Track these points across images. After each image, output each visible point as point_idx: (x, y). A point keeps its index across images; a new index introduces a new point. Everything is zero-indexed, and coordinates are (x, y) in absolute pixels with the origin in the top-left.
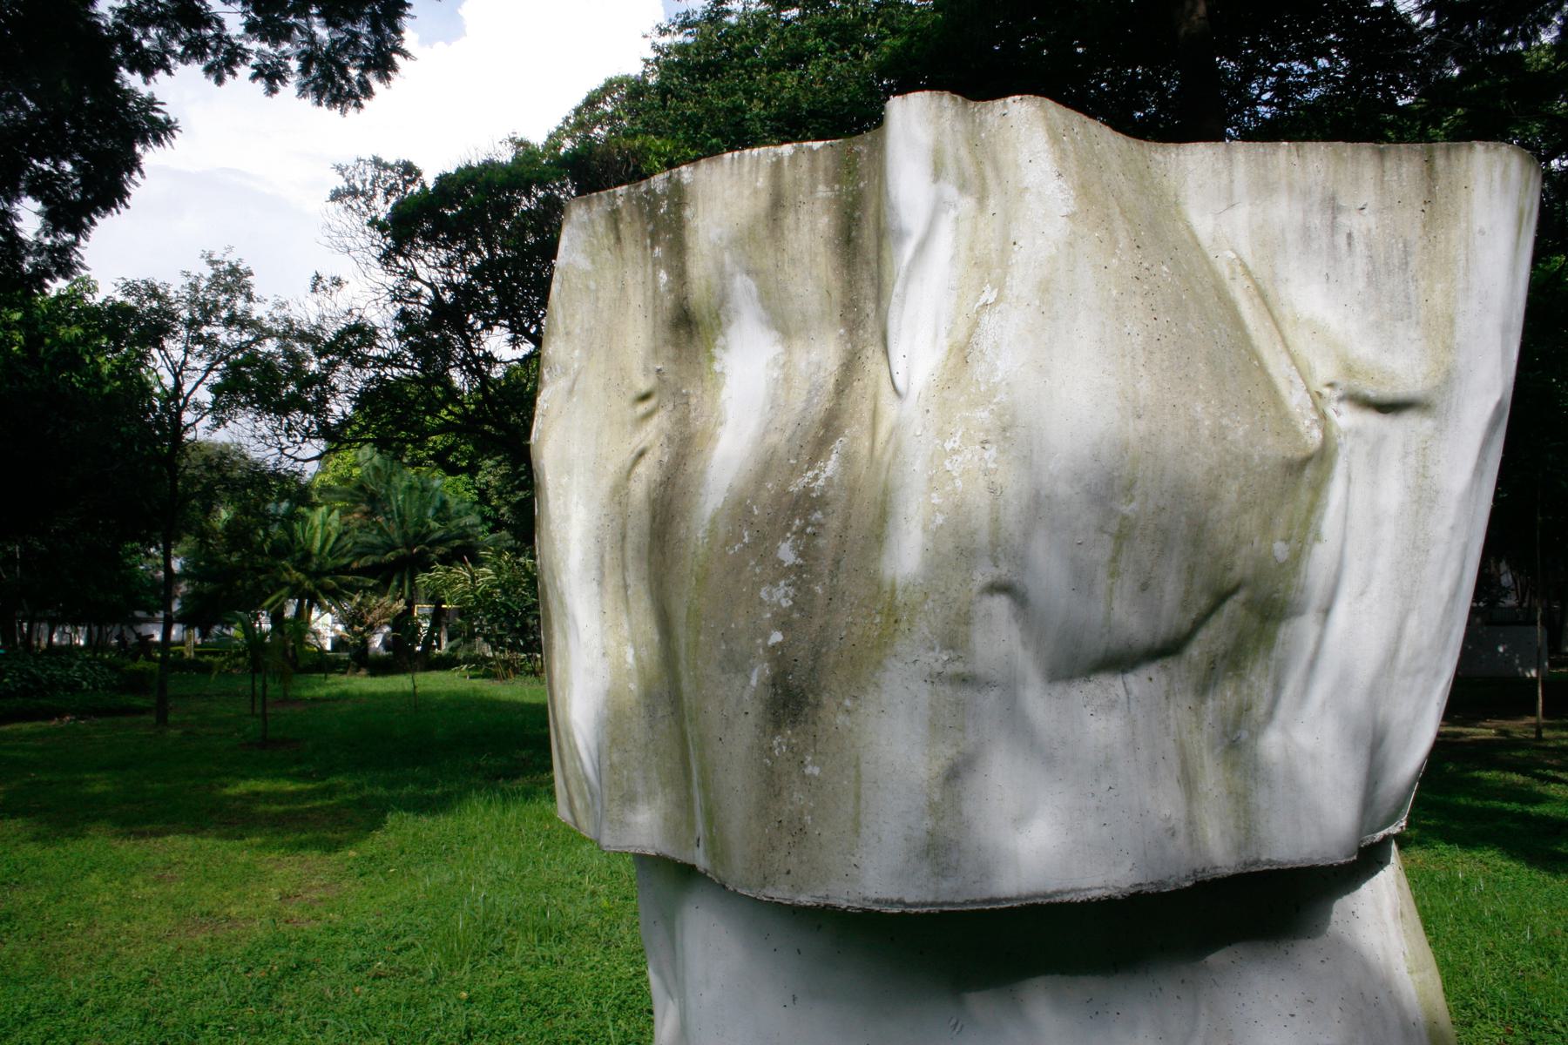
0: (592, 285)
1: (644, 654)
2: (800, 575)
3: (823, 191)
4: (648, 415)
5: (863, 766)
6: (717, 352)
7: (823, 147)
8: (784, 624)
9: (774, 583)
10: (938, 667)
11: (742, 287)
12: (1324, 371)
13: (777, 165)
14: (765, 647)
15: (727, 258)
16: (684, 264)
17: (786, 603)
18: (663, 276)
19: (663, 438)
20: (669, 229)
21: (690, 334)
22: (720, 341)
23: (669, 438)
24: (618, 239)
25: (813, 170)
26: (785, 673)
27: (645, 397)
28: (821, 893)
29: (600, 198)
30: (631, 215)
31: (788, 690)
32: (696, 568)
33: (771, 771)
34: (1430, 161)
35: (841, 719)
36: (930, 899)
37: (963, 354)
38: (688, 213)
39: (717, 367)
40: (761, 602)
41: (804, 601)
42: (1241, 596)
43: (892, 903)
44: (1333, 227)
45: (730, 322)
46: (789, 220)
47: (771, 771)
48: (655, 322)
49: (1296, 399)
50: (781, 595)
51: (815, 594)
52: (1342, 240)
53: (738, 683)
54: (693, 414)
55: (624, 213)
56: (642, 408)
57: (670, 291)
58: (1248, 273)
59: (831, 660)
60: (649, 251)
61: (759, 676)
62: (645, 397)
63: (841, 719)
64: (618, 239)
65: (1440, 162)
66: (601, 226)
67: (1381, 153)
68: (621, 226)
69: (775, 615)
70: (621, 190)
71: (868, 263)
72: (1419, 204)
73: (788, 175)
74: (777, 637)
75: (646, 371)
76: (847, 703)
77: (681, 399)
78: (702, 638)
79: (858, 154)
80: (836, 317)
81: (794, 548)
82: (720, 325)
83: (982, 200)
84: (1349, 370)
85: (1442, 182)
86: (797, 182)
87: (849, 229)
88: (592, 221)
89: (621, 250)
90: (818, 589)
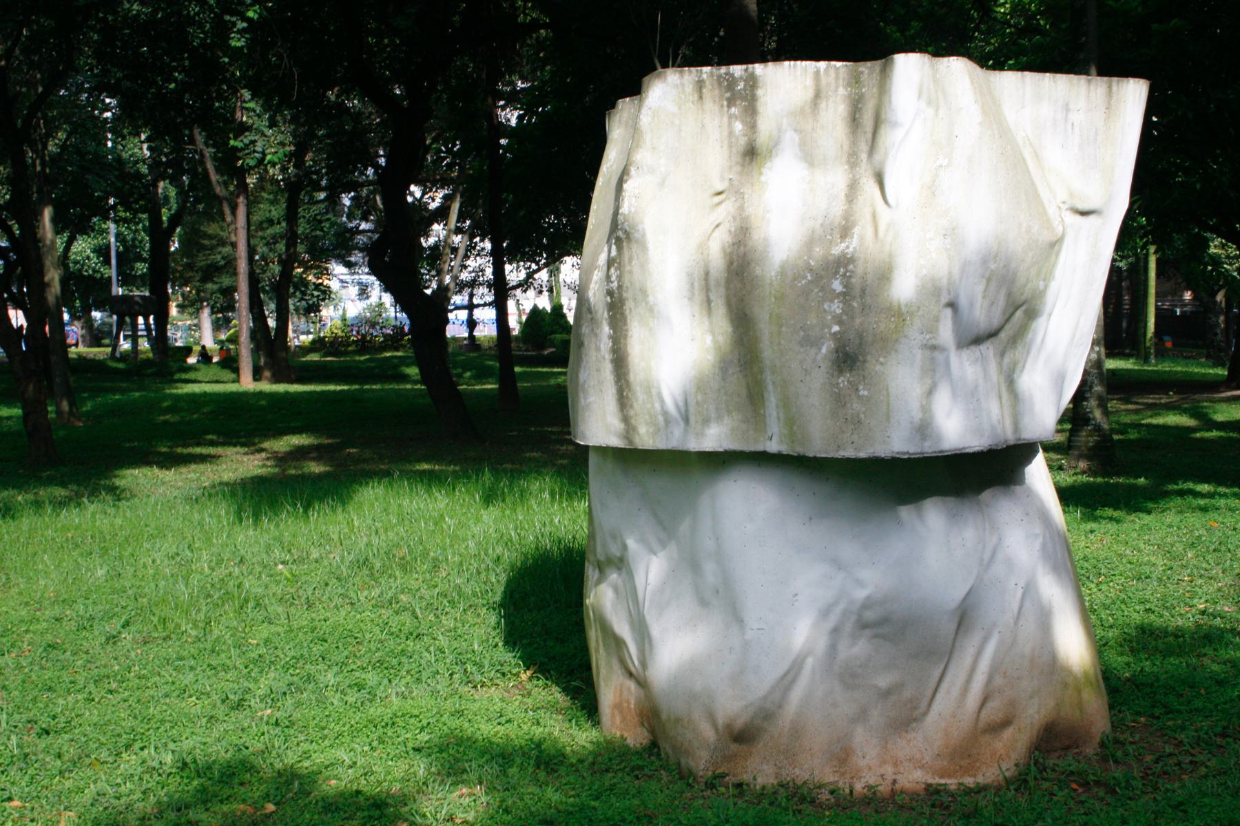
0: (677, 122)
1: (721, 339)
2: (846, 296)
3: (842, 91)
4: (719, 203)
5: (890, 390)
6: (764, 170)
7: (843, 66)
8: (840, 323)
9: (832, 301)
10: (925, 342)
11: (790, 139)
12: (1062, 195)
13: (817, 73)
14: (830, 334)
15: (785, 121)
16: (755, 121)
17: (839, 311)
18: (738, 126)
19: (730, 218)
20: (744, 99)
21: (751, 160)
22: (768, 165)
23: (734, 218)
24: (701, 98)
25: (837, 78)
26: (844, 346)
27: (720, 193)
28: (872, 451)
29: (690, 71)
30: (712, 85)
31: (846, 355)
32: (773, 292)
33: (838, 395)
34: (1110, 87)
35: (878, 367)
36: (919, 451)
37: (932, 190)
38: (759, 92)
39: (763, 178)
40: (825, 311)
41: (848, 311)
42: (1023, 308)
43: (904, 453)
44: (1066, 119)
45: (777, 155)
46: (823, 105)
47: (838, 395)
48: (731, 152)
49: (1052, 211)
50: (836, 307)
51: (854, 307)
52: (1069, 126)
53: (813, 351)
54: (746, 204)
55: (707, 83)
56: (717, 199)
57: (745, 135)
58: (1031, 144)
59: (870, 339)
60: (726, 109)
61: (827, 348)
62: (720, 193)
63: (878, 367)
64: (701, 98)
65: (1114, 88)
66: (689, 88)
67: (1089, 81)
68: (704, 91)
69: (833, 317)
70: (706, 69)
71: (865, 133)
72: (1103, 109)
73: (824, 81)
74: (836, 328)
75: (722, 179)
76: (881, 359)
77: (740, 194)
78: (783, 329)
79: (862, 73)
80: (844, 159)
81: (841, 283)
82: (770, 156)
83: (937, 110)
84: (1072, 195)
85: (1114, 99)
86: (828, 85)
87: (854, 113)
88: (683, 85)
89: (702, 104)
90: (855, 304)
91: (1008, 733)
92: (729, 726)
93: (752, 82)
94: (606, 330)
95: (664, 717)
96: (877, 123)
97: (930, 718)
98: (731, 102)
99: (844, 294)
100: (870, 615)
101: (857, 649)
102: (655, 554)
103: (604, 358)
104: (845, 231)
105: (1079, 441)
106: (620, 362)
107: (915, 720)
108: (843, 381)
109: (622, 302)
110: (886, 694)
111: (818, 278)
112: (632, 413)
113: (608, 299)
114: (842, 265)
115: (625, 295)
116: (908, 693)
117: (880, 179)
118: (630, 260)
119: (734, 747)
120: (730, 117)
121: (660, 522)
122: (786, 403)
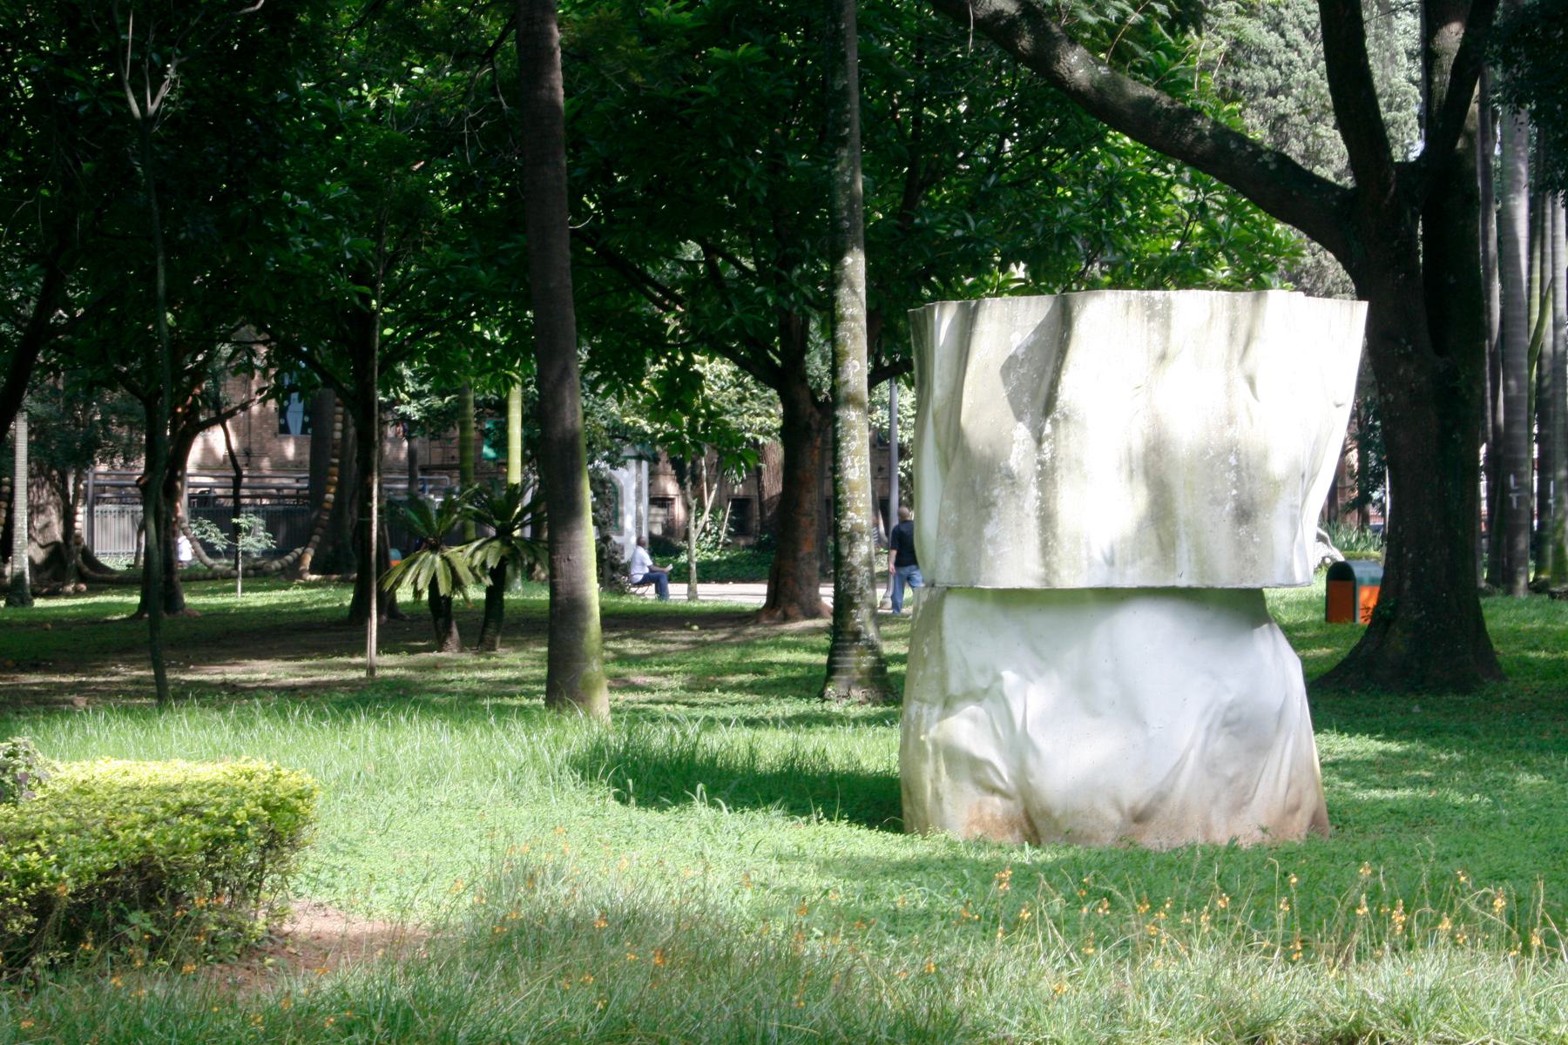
18: (1156, 337)
20: (1162, 317)
38: (1173, 313)
53: (1219, 509)
74: (1234, 492)
91: (1299, 815)
92: (1132, 809)
93: (1168, 304)
94: (1034, 492)
95: (1057, 814)
96: (1249, 339)
97: (1255, 803)
98: (1150, 318)
99: (1237, 466)
100: (1232, 716)
101: (1220, 744)
102: (1032, 681)
103: (1028, 515)
104: (1231, 421)
105: (849, 662)
106: (1047, 519)
107: (1245, 804)
108: (1242, 531)
109: (1054, 469)
110: (1231, 781)
111: (1218, 455)
112: (1055, 559)
113: (1039, 467)
114: (1232, 448)
115: (1057, 464)
116: (1242, 782)
117: (1251, 382)
118: (1067, 437)
119: (1134, 826)
120: (1149, 330)
121: (1035, 650)
122: (1198, 548)
